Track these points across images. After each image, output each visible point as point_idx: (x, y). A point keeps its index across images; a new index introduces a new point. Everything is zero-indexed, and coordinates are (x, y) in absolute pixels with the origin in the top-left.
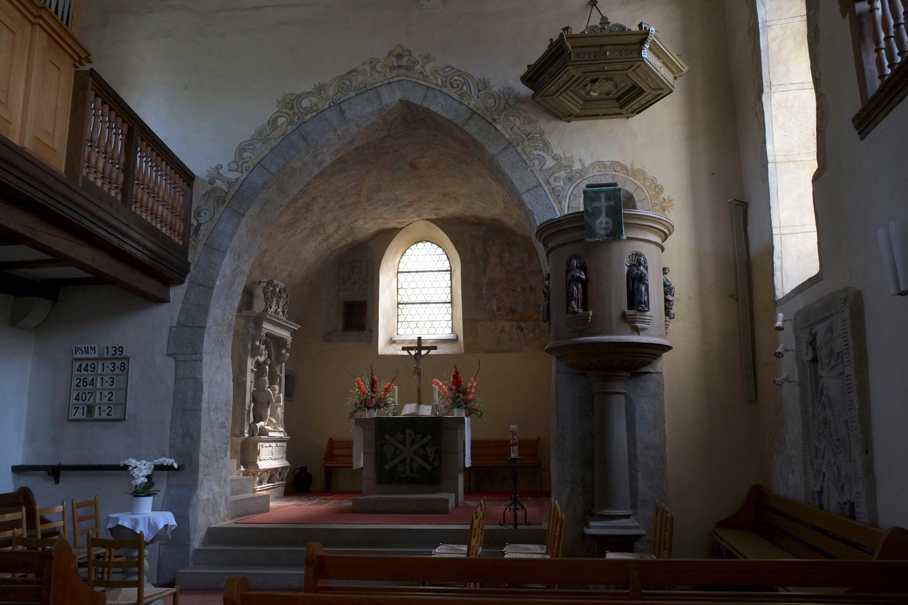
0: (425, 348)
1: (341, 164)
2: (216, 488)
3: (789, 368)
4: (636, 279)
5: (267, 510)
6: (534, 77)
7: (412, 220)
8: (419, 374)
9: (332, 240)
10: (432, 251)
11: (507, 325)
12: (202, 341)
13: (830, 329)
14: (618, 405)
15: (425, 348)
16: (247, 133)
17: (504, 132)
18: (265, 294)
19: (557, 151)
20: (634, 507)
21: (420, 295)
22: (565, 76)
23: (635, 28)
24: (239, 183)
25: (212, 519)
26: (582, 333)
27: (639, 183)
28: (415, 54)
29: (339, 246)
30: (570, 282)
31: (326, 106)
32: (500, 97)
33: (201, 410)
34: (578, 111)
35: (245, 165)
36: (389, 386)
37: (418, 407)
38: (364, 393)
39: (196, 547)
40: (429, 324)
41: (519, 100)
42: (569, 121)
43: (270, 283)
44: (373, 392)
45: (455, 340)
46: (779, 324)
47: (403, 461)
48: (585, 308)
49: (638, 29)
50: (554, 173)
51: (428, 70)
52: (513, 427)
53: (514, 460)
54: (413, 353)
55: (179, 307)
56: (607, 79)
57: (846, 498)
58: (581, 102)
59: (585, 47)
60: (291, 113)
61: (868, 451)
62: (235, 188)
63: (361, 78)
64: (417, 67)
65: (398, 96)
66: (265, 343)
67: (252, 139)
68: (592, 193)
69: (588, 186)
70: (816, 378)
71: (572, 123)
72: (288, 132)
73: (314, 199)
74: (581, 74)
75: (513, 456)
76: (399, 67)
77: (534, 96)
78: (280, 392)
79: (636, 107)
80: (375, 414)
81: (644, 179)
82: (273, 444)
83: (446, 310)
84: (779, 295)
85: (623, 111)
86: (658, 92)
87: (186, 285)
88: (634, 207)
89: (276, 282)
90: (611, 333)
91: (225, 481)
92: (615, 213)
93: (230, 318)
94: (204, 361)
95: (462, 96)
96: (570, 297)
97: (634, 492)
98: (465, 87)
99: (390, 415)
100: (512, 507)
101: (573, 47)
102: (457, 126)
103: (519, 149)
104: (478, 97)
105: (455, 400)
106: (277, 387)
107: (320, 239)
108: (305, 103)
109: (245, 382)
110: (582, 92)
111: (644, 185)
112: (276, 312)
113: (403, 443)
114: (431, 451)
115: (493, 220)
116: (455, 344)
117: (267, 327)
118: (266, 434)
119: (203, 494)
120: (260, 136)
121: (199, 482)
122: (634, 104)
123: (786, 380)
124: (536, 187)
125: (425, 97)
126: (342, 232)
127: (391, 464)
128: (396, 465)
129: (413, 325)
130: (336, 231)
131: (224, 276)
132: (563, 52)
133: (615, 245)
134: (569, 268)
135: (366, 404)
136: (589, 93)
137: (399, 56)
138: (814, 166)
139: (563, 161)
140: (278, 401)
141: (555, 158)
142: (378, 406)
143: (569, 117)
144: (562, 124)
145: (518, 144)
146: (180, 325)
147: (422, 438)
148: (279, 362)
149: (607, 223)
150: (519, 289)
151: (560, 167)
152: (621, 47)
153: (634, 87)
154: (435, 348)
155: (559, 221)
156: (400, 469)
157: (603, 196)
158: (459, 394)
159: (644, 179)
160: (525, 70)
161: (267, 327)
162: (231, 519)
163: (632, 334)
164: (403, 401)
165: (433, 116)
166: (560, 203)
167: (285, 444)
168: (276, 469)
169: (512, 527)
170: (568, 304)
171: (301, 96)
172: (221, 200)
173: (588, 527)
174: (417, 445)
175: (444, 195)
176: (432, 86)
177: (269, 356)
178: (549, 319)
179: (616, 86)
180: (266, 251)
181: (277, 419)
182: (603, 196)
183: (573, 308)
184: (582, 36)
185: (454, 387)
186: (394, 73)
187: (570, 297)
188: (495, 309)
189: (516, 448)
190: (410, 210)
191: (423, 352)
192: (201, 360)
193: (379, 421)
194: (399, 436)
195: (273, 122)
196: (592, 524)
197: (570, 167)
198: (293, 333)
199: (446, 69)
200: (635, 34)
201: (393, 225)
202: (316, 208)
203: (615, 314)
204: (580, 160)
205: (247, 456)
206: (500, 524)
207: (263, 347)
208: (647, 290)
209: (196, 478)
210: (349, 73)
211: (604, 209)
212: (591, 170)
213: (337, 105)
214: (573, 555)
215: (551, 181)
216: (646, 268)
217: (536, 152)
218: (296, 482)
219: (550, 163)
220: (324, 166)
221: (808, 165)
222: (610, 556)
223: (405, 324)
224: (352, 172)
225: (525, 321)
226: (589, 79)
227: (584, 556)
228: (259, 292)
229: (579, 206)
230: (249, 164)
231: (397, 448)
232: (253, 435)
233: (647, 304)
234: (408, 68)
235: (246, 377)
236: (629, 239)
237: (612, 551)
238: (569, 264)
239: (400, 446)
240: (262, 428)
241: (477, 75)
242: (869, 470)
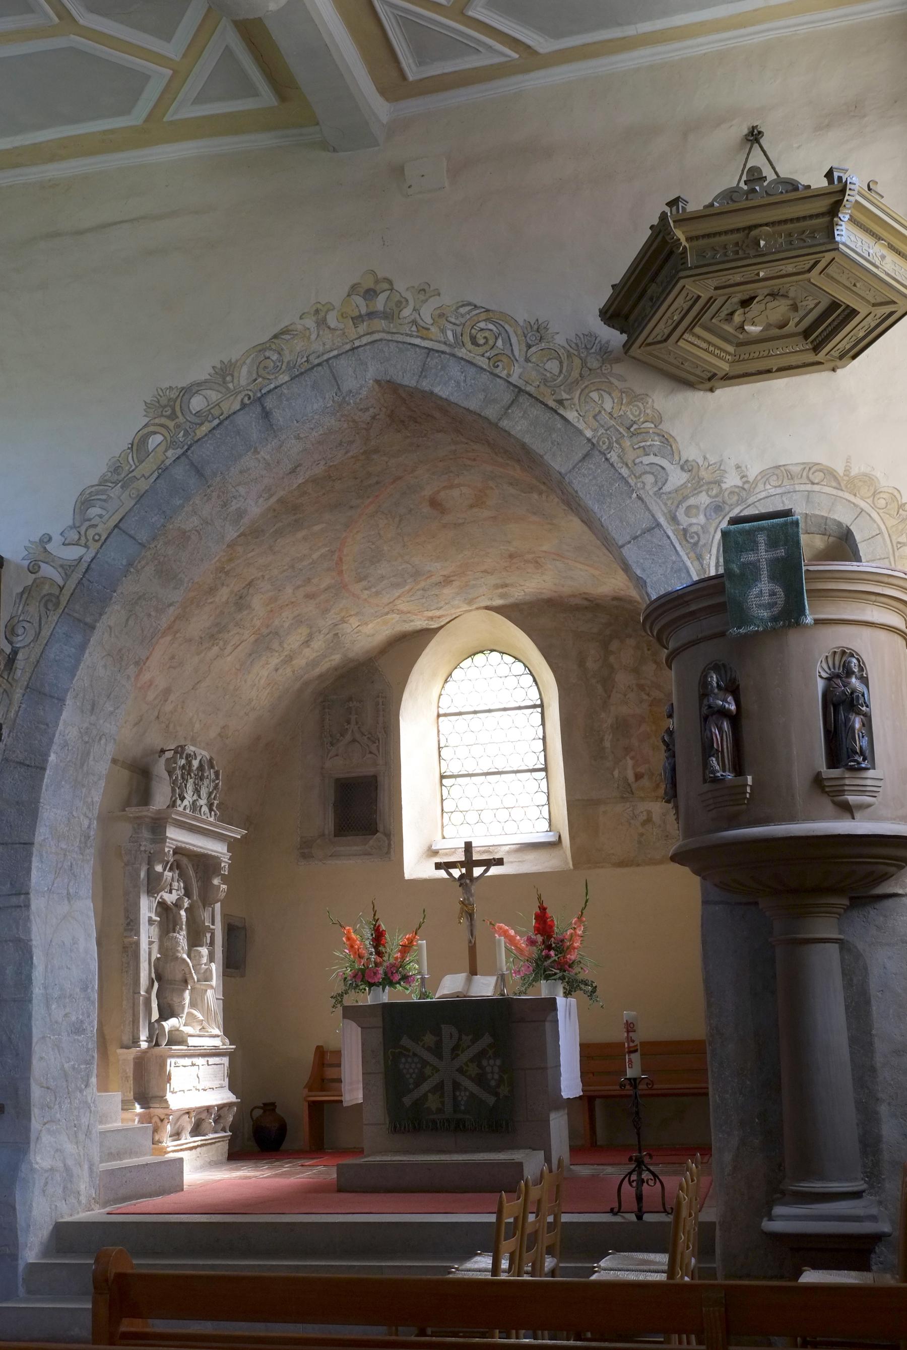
0: (479, 863)
1: (289, 513)
2: (70, 1148)
4: (843, 705)
5: (179, 1188)
6: (630, 306)
7: (458, 611)
8: (471, 916)
9: (299, 662)
10: (503, 670)
12: (29, 870)
14: (825, 966)
15: (479, 863)
16: (93, 468)
17: (581, 426)
18: (170, 773)
19: (690, 453)
20: (873, 1175)
21: (482, 761)
22: (680, 300)
23: (819, 182)
24: (84, 566)
25: (63, 1207)
26: (734, 821)
27: (862, 504)
29: (317, 671)
30: (706, 719)
31: (237, 406)
32: (569, 355)
33: (30, 1001)
34: (726, 367)
35: (91, 532)
36: (411, 941)
37: (469, 981)
38: (361, 957)
39: (31, 1260)
40: (503, 815)
41: (605, 354)
42: (712, 390)
43: (180, 750)
44: (379, 954)
45: (558, 842)
48: (739, 769)
49: (824, 183)
50: (685, 498)
51: (426, 314)
53: (634, 1082)
54: (456, 873)
56: (773, 295)
58: (731, 349)
59: (715, 235)
60: (171, 424)
62: (77, 576)
63: (299, 345)
64: (406, 312)
65: (372, 372)
66: (176, 865)
67: (103, 482)
68: (740, 535)
69: (734, 521)
71: (718, 392)
72: (168, 462)
73: (250, 584)
74: (712, 292)
75: (630, 1073)
76: (371, 315)
77: (627, 346)
78: (211, 958)
79: (846, 345)
80: (386, 996)
81: (874, 495)
82: (201, 1061)
83: (535, 784)
85: (821, 356)
86: (887, 309)
88: (859, 559)
89: (190, 749)
90: (792, 819)
91: (88, 1133)
92: (788, 570)
93: (86, 822)
94: (33, 907)
95: (495, 360)
96: (708, 749)
97: (870, 1144)
98: (500, 343)
99: (415, 999)
100: (634, 1177)
101: (689, 239)
102: (490, 422)
103: (613, 456)
104: (527, 360)
106: (204, 951)
107: (275, 661)
108: (197, 403)
109: (137, 944)
110: (728, 328)
111: (874, 507)
112: (194, 806)
113: (437, 1051)
114: (492, 1066)
115: (615, 598)
116: (555, 852)
117: (176, 836)
118: (182, 1042)
119: (42, 1158)
120: (118, 475)
121: (33, 1136)
122: (842, 340)
124: (649, 530)
125: (424, 371)
126: (318, 644)
127: (416, 1095)
128: (425, 1095)
129: (472, 817)
130: (307, 643)
131: (65, 745)
132: (671, 253)
133: (794, 638)
134: (705, 692)
136: (741, 328)
137: (370, 294)
139: (703, 473)
140: (207, 977)
143: (710, 381)
144: (697, 398)
145: (610, 448)
147: (474, 1041)
148: (206, 899)
149: (772, 594)
151: (697, 485)
152: (790, 226)
153: (835, 305)
154: (500, 862)
155: (684, 595)
156: (433, 1103)
157: (762, 539)
158: (550, 953)
159: (874, 495)
160: (607, 293)
161: (176, 836)
162: (104, 1205)
163: (836, 818)
165: (444, 406)
166: (699, 558)
167: (225, 1060)
168: (208, 1109)
169: (632, 1217)
170: (706, 764)
171: (188, 391)
172: (51, 601)
173: (771, 1219)
175: (511, 556)
176: (436, 346)
177: (188, 894)
178: (675, 796)
179: (795, 307)
180: (167, 691)
181: (207, 1012)
182: (762, 539)
183: (714, 772)
184: (709, 213)
185: (540, 938)
186: (363, 328)
187: (708, 749)
188: (631, 777)
189: (636, 1057)
190: (447, 591)
191: (477, 871)
192: (28, 906)
194: (429, 1039)
195: (139, 446)
196: (778, 1210)
197: (718, 483)
198: (233, 845)
199: (463, 310)
200: (820, 195)
201: (419, 623)
202: (257, 602)
203: (800, 781)
204: (738, 467)
205: (147, 1088)
206: (612, 1211)
207: (168, 874)
208: (868, 723)
209: (27, 1129)
210: (276, 337)
211: (764, 565)
212: (761, 486)
213: (258, 403)
214: (748, 1276)
215: (681, 515)
216: (865, 681)
217: (647, 460)
218: (255, 1133)
219: (677, 478)
220: (246, 521)
222: (810, 1277)
223: (457, 818)
224: (317, 528)
226: (735, 300)
227: (771, 1278)
228: (160, 768)
229: (712, 565)
230: (99, 529)
231: (425, 1063)
232: (157, 1044)
233: (868, 755)
234: (388, 316)
235: (138, 933)
236: (817, 622)
237: (815, 1267)
238: (704, 684)
240: (174, 1031)
241: (522, 316)
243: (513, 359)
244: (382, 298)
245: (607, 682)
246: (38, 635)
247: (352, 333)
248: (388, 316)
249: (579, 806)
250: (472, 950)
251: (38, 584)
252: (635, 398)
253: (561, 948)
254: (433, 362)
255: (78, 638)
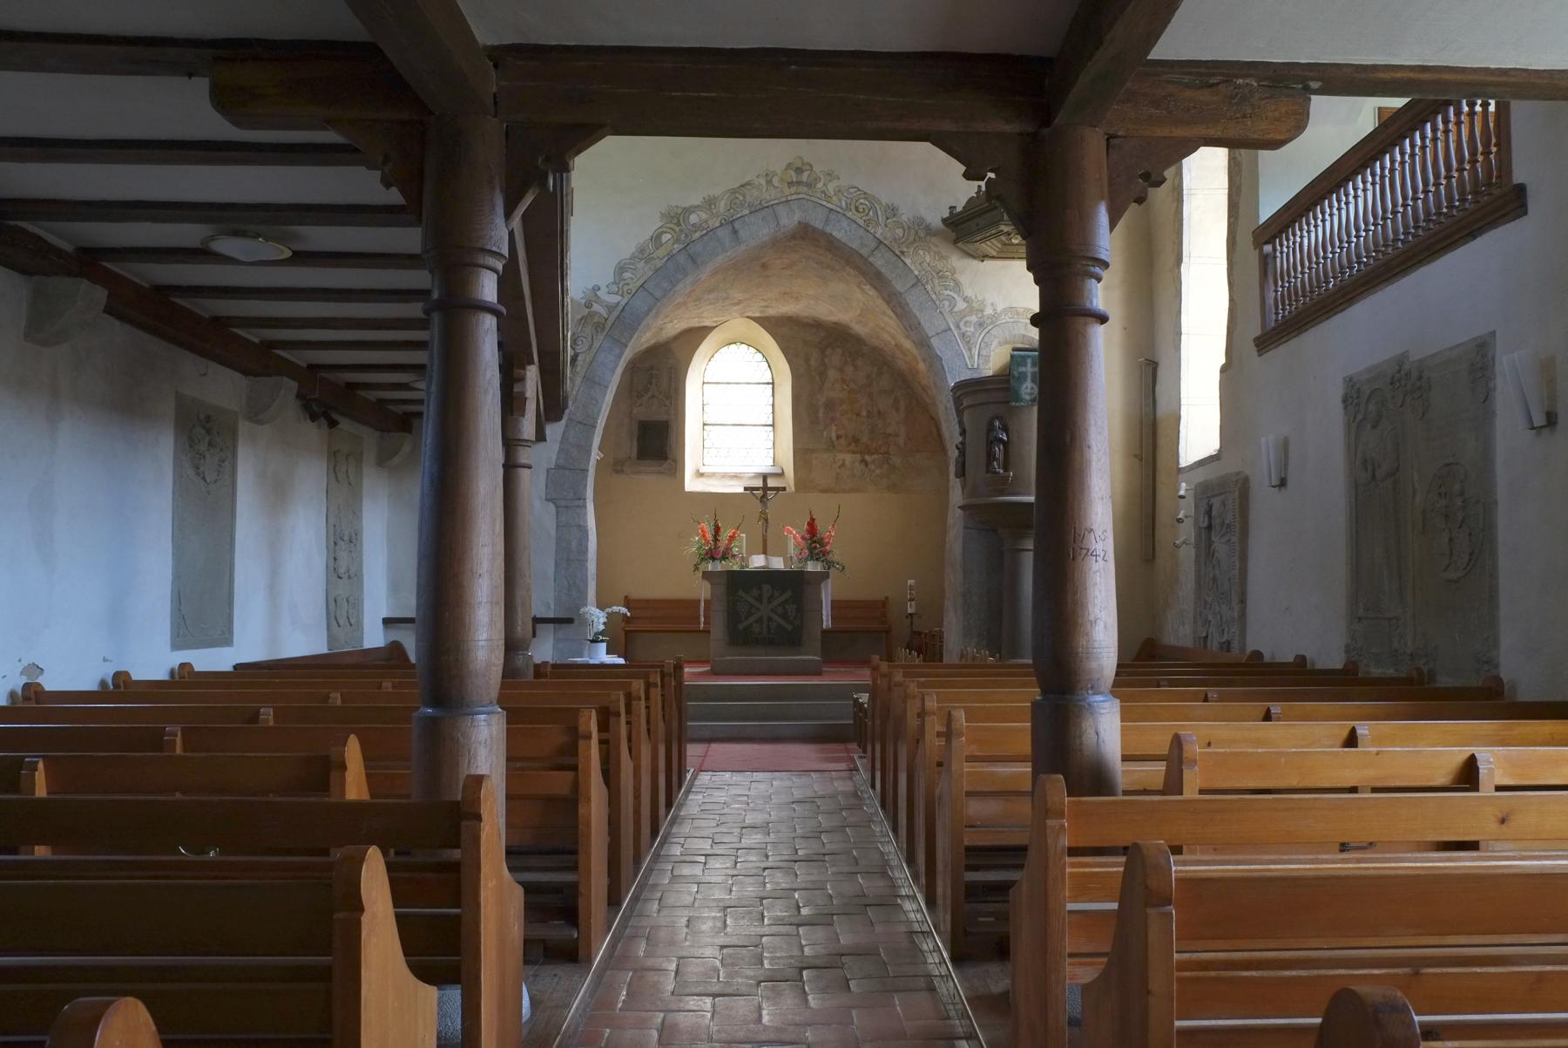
3: (1187, 532)
11: (848, 458)
13: (1224, 504)
16: (627, 249)
19: (969, 293)
26: (1002, 493)
28: (817, 169)
46: (1182, 493)
47: (760, 621)
48: (1006, 469)
51: (831, 188)
52: (911, 582)
55: (556, 447)
57: (1225, 638)
61: (1243, 601)
62: (616, 314)
63: (755, 193)
64: (820, 185)
69: (1015, 349)
70: (1210, 543)
76: (799, 183)
84: (1183, 463)
87: (563, 422)
103: (929, 287)
105: (811, 550)
108: (693, 219)
113: (759, 599)
120: (642, 254)
123: (1184, 542)
125: (827, 221)
127: (746, 623)
134: (991, 428)
135: (711, 555)
137: (799, 171)
138: (1223, 360)
141: (965, 299)
142: (724, 557)
143: (984, 257)
144: (975, 263)
146: (558, 467)
150: (864, 413)
157: (1029, 361)
158: (814, 543)
164: (751, 552)
172: (599, 327)
174: (775, 603)
182: (1029, 361)
186: (793, 190)
187: (990, 457)
193: (731, 574)
194: (755, 592)
195: (656, 239)
201: (708, 323)
213: (730, 223)
219: (961, 305)
221: (1217, 355)
225: (871, 453)
234: (809, 185)
239: (756, 604)
242: (1243, 614)
243: (878, 224)
244: (806, 174)
245: (823, 375)
246: (591, 347)
247: (787, 191)
248: (809, 185)
249: (802, 453)
250: (765, 541)
251: (592, 315)
252: (942, 257)
253: (821, 542)
254: (832, 217)
255: (617, 351)
